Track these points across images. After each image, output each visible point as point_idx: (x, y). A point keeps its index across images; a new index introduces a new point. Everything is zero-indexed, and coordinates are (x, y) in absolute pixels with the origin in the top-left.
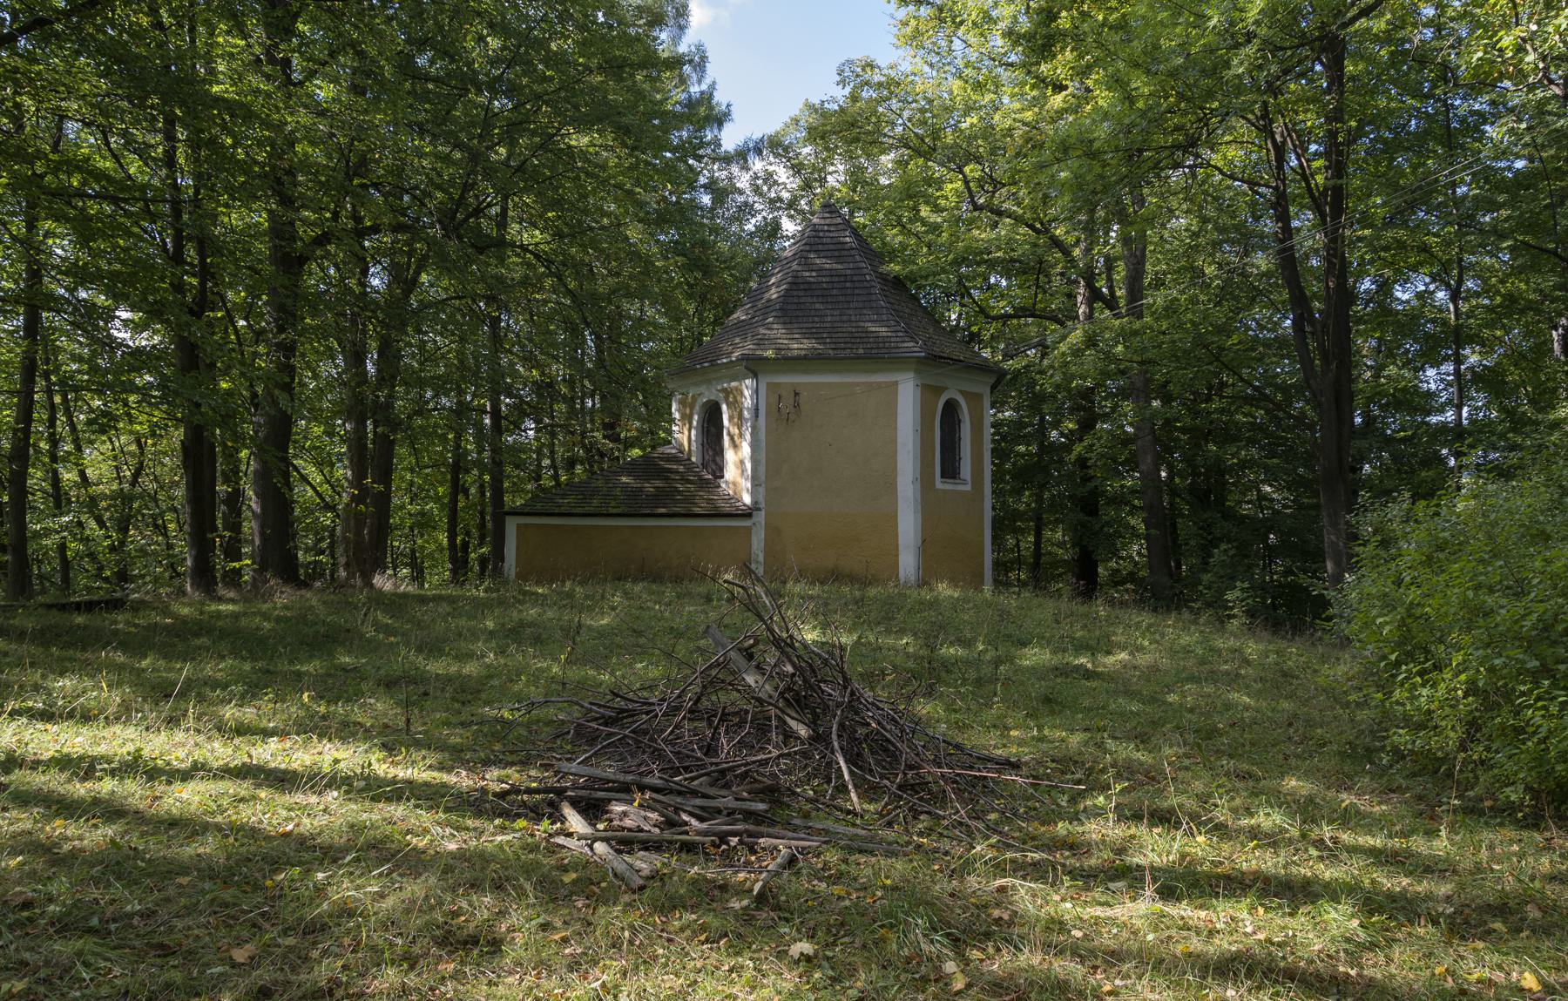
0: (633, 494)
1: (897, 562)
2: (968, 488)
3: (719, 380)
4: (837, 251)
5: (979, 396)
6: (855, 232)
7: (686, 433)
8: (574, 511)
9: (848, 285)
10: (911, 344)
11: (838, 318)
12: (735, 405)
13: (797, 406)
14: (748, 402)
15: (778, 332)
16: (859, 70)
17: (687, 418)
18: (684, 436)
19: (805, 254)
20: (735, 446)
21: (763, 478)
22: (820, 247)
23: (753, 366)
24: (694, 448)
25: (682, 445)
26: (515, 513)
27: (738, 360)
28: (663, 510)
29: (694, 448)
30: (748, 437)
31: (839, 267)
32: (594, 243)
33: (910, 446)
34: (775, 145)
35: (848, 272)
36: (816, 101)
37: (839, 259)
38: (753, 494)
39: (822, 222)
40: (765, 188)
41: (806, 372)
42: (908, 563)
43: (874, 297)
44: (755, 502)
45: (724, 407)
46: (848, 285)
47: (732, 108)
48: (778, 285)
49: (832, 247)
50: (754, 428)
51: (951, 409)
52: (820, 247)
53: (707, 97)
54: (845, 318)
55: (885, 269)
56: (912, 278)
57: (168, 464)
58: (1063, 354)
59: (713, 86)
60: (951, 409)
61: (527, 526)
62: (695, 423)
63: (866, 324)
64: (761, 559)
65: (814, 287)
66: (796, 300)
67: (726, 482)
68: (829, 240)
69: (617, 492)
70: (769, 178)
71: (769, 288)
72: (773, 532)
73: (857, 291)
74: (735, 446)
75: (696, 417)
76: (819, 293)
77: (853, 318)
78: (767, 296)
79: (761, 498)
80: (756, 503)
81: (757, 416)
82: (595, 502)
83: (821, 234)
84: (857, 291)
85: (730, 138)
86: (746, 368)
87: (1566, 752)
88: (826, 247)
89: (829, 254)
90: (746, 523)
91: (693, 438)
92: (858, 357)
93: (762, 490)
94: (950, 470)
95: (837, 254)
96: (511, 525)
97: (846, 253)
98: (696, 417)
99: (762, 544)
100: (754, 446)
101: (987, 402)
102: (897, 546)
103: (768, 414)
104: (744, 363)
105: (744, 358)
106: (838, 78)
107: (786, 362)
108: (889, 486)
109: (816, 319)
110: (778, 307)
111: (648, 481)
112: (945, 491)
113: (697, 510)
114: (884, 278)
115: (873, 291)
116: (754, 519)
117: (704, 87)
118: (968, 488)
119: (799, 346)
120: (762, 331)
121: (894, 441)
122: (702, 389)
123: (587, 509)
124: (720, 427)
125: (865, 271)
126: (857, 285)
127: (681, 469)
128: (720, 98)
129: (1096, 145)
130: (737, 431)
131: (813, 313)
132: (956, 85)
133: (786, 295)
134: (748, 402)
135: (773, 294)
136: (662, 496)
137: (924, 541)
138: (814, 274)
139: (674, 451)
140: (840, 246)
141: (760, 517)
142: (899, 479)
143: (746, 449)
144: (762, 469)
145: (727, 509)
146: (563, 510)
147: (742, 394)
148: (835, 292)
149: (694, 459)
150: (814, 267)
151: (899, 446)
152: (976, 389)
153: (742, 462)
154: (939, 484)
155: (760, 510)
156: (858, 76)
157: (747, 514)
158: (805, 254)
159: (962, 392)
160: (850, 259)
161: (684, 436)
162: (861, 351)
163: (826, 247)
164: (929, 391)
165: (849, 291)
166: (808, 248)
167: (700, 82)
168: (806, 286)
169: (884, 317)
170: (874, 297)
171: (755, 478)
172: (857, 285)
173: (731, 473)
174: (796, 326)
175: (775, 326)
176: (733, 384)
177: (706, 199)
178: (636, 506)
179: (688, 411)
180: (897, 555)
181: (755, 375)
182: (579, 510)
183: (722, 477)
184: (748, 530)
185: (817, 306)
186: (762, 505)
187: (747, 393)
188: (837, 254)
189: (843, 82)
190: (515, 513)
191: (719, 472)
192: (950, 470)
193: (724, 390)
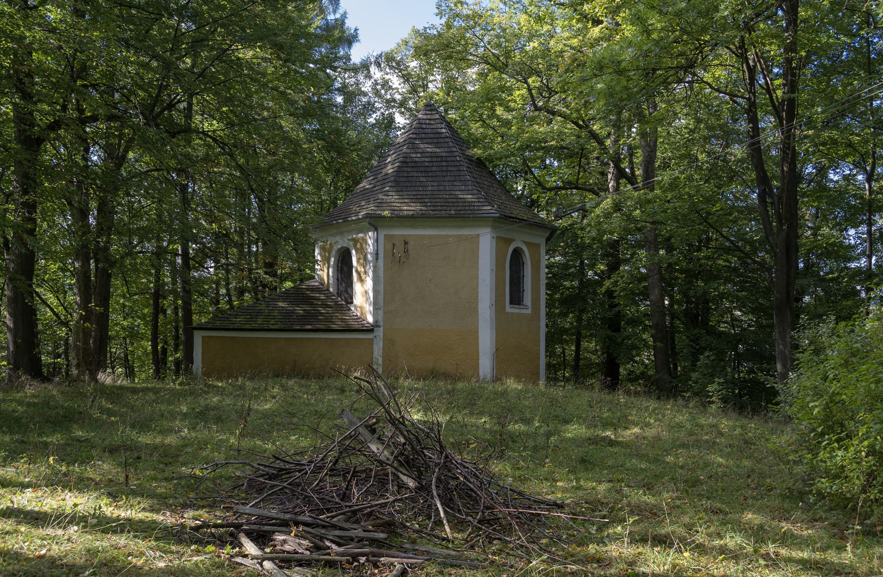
0: (287, 315)
1: (478, 364)
3: (350, 232)
4: (436, 139)
6: (449, 125)
7: (326, 271)
8: (244, 327)
9: (444, 164)
10: (489, 208)
11: (436, 188)
12: (361, 251)
13: (406, 251)
14: (370, 249)
15: (393, 198)
16: (452, 5)
17: (326, 260)
18: (325, 273)
19: (412, 141)
20: (361, 280)
21: (382, 304)
22: (423, 136)
23: (374, 222)
24: (331, 282)
25: (322, 279)
26: (201, 328)
27: (363, 218)
28: (309, 327)
30: (371, 274)
31: (437, 150)
33: (488, 282)
34: (389, 60)
35: (444, 154)
36: (420, 28)
37: (437, 145)
38: (374, 316)
39: (425, 117)
40: (383, 92)
41: (413, 227)
42: (486, 365)
43: (462, 173)
44: (376, 321)
45: (354, 252)
46: (444, 164)
47: (359, 32)
49: (432, 136)
50: (375, 267)
51: (517, 254)
52: (423, 136)
53: (340, 23)
54: (441, 188)
55: (470, 152)
56: (490, 159)
58: (598, 216)
59: (344, 16)
60: (517, 254)
61: (209, 337)
63: (457, 193)
65: (419, 164)
66: (405, 174)
67: (356, 307)
70: (386, 84)
72: (389, 342)
73: (450, 168)
74: (361, 280)
75: (333, 259)
76: (422, 169)
77: (447, 188)
78: (384, 171)
79: (380, 318)
80: (377, 322)
81: (377, 259)
82: (259, 321)
83: (424, 126)
84: (450, 168)
85: (357, 54)
86: (370, 224)
88: (428, 136)
89: (430, 141)
90: (370, 336)
91: (331, 274)
92: (451, 217)
93: (381, 312)
94: (516, 299)
95: (435, 141)
96: (198, 338)
97: (442, 140)
98: (333, 259)
99: (381, 352)
101: (543, 250)
103: (384, 258)
104: (368, 220)
105: (368, 216)
106: (437, 11)
107: (399, 219)
108: (473, 310)
109: (421, 189)
110: (392, 179)
111: (298, 305)
112: (512, 314)
113: (335, 327)
114: (470, 159)
115: (461, 168)
116: (375, 333)
117: (338, 16)
118: (529, 311)
119: (409, 208)
120: (381, 196)
121: (477, 277)
122: (338, 238)
124: (351, 266)
125: (456, 154)
126: (450, 164)
127: (322, 297)
128: (350, 24)
129: (623, 65)
131: (418, 184)
132: (523, 18)
133: (399, 171)
134: (370, 249)
135: (390, 169)
137: (497, 349)
138: (419, 155)
139: (316, 284)
140: (437, 136)
141: (379, 332)
143: (369, 283)
144: (381, 298)
145: (357, 327)
146: (236, 326)
147: (366, 243)
148: (434, 169)
149: (331, 290)
150: (420, 150)
152: (535, 240)
153: (366, 292)
154: (509, 309)
155: (379, 326)
156: (451, 10)
157: (370, 330)
158: (412, 141)
159: (525, 242)
160: (445, 145)
161: (325, 273)
162: (453, 212)
163: (428, 136)
164: (502, 242)
165: (444, 169)
166: (414, 136)
167: (335, 12)
168: (413, 165)
169: (470, 188)
170: (462, 173)
171: (375, 304)
172: (450, 164)
174: (406, 193)
175: (391, 193)
176: (360, 235)
177: (339, 99)
178: (288, 324)
179: (327, 254)
181: (376, 229)
182: (248, 326)
183: (352, 303)
184: (371, 341)
185: (422, 179)
186: (381, 323)
187: (370, 242)
188: (435, 141)
189: (440, 14)
190: (201, 328)
191: (349, 300)
192: (516, 299)
193: (353, 240)
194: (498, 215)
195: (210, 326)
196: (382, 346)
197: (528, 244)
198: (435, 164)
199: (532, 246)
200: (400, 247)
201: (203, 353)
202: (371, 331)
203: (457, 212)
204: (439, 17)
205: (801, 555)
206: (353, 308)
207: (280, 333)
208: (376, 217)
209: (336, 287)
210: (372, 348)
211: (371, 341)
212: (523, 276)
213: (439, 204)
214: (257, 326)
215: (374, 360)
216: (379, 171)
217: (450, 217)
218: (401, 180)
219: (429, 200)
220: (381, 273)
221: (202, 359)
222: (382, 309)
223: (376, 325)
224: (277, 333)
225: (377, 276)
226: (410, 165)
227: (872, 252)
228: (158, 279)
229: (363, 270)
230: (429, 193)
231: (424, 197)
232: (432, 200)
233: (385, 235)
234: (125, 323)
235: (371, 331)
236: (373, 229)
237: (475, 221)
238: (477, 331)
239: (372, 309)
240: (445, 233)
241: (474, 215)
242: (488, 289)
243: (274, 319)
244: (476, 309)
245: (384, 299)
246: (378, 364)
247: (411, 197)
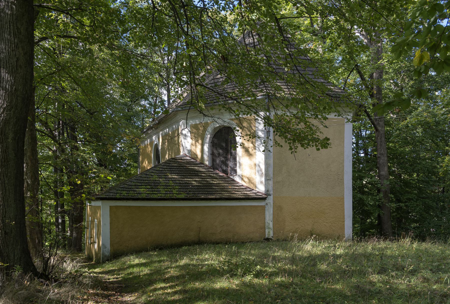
1: (344, 224)
7: (199, 147)
21: (272, 175)
29: (206, 157)
38: (266, 185)
44: (267, 191)
57: (432, 180)
61: (116, 207)
62: (208, 140)
64: (271, 226)
72: (278, 209)
79: (271, 188)
87: (246, 1)
90: (262, 203)
93: (271, 182)
99: (271, 217)
116: (267, 201)
141: (270, 200)
145: (239, 194)
154: (93, 262)
155: (270, 195)
184: (263, 208)
186: (271, 193)
196: (272, 212)
202: (264, 199)
205: (261, 282)
206: (237, 179)
215: (266, 224)
221: (111, 228)
222: (272, 180)
223: (267, 194)
229: (251, 145)
234: (159, 8)
235: (264, 199)
239: (263, 179)
244: (343, 179)
245: (274, 171)
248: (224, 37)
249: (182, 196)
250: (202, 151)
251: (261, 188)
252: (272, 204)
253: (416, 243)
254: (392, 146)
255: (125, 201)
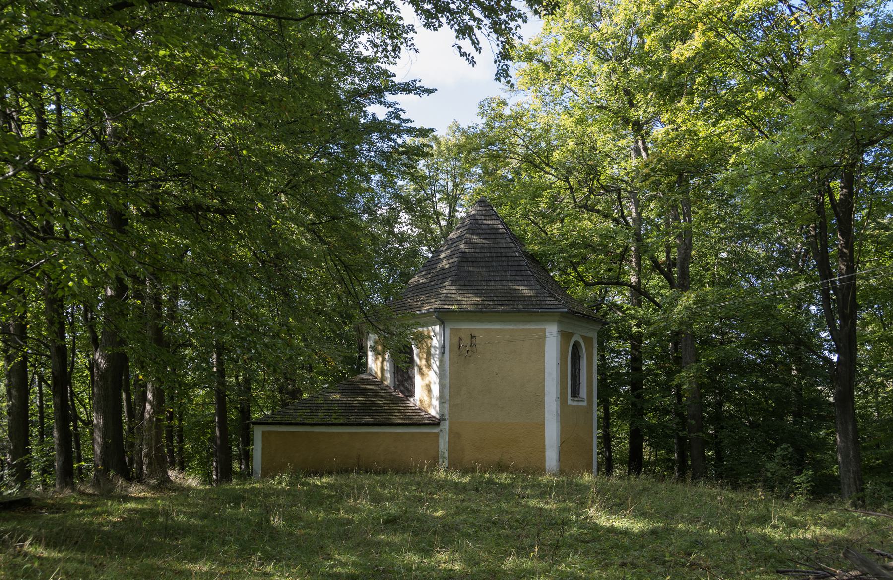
1: (544, 456)
2: (585, 404)
4: (492, 233)
5: (591, 339)
8: (335, 421)
9: (503, 259)
21: (448, 397)
23: (442, 317)
26: (259, 423)
28: (368, 419)
30: (435, 367)
32: (22, 317)
36: (464, 125)
41: (480, 321)
42: (552, 458)
46: (503, 259)
48: (448, 258)
49: (488, 231)
50: (441, 361)
59: (373, 115)
63: (521, 288)
64: (446, 455)
65: (479, 259)
68: (486, 227)
69: (336, 407)
71: (441, 260)
72: (455, 436)
73: (510, 264)
74: (422, 374)
79: (446, 412)
80: (443, 415)
81: (443, 353)
82: (321, 415)
84: (510, 264)
86: (436, 317)
90: (436, 430)
93: (447, 406)
94: (575, 393)
95: (493, 236)
96: (258, 433)
97: (499, 236)
100: (441, 376)
102: (544, 445)
103: (451, 351)
104: (436, 314)
107: (464, 314)
108: (540, 403)
109: (484, 283)
112: (574, 406)
114: (525, 253)
116: (441, 427)
118: (585, 404)
119: (470, 300)
121: (543, 371)
123: (316, 420)
130: (424, 362)
131: (480, 279)
136: (366, 408)
137: (562, 443)
140: (494, 231)
141: (445, 425)
142: (547, 399)
143: (432, 377)
145: (416, 419)
146: (298, 420)
151: (546, 375)
152: (590, 335)
154: (570, 402)
155: (445, 420)
157: (435, 423)
162: (521, 307)
163: (484, 232)
164: (565, 336)
168: (473, 259)
173: (419, 393)
180: (544, 452)
181: (442, 323)
182: (310, 421)
184: (437, 435)
186: (447, 417)
188: (493, 236)
189: (482, 114)
190: (259, 423)
191: (409, 392)
192: (575, 393)
194: (566, 310)
195: (270, 420)
196: (447, 439)
197: (584, 338)
198: (494, 259)
199: (587, 340)
200: (466, 341)
201: (263, 449)
203: (525, 306)
204: (480, 117)
207: (344, 427)
208: (448, 312)
209: (393, 381)
210: (438, 441)
211: (437, 434)
212: (580, 369)
213: (506, 299)
214: (319, 421)
216: (434, 266)
217: (519, 312)
218: (462, 274)
219: (495, 295)
220: (447, 366)
221: (263, 454)
222: (448, 402)
224: (340, 427)
225: (443, 370)
226: (470, 260)
227: (596, 321)
228: (382, 397)
230: (492, 287)
231: (489, 291)
232: (498, 295)
233: (451, 329)
235: (438, 424)
236: (439, 322)
237: (542, 315)
238: (543, 425)
240: (511, 328)
241: (542, 310)
242: (555, 382)
243: (335, 413)
246: (443, 458)
247: (476, 291)
248: (195, 83)
249: (340, 421)
250: (382, 369)
251: (433, 412)
252: (448, 430)
253: (736, 15)
254: (165, 56)
255: (278, 426)
